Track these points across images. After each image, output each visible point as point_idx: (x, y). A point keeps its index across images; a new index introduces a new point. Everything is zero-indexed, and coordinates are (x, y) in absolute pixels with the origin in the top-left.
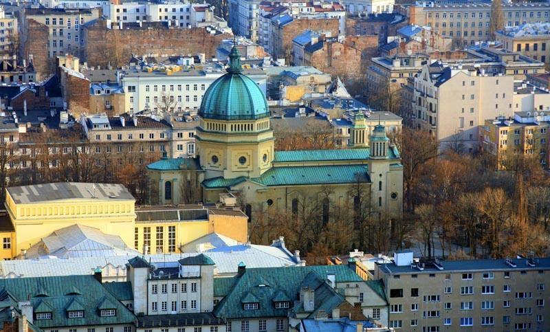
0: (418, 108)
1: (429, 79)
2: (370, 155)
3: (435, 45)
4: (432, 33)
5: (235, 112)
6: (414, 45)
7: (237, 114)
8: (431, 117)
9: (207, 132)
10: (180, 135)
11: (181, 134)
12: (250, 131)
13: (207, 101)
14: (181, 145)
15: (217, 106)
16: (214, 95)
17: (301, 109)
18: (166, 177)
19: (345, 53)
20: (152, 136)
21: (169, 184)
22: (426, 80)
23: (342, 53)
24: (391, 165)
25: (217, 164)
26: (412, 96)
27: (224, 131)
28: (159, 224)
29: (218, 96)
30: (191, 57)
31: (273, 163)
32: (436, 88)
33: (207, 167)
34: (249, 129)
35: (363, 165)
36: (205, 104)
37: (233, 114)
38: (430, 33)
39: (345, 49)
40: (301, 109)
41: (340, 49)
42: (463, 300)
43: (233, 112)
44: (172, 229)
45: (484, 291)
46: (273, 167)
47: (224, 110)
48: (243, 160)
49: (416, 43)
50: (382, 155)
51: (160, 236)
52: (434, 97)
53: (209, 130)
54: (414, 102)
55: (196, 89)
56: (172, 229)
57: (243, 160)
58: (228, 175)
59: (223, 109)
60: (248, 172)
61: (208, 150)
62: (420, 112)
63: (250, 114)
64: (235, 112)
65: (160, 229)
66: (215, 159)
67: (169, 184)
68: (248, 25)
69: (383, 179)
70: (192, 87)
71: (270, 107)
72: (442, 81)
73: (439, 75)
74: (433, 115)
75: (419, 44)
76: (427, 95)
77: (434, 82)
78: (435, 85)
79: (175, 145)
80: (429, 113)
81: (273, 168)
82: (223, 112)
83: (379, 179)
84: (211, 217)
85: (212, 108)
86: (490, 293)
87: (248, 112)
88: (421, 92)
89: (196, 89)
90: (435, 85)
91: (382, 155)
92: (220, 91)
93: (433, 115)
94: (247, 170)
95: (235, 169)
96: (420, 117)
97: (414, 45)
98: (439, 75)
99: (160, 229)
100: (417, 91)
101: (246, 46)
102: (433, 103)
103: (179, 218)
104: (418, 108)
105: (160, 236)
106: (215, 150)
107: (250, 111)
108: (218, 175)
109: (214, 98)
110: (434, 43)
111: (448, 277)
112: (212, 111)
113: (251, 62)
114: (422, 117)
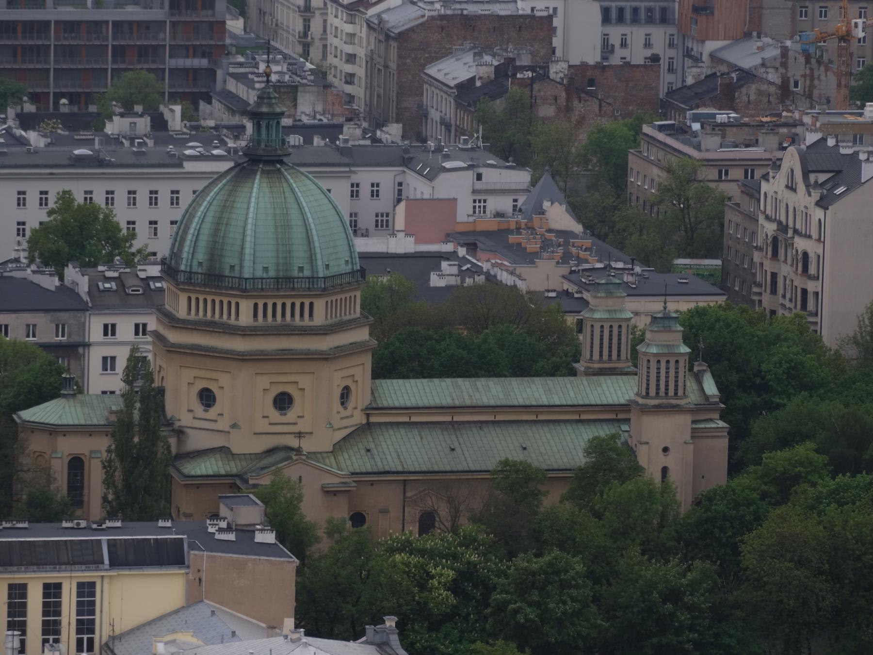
0: (769, 266)
1: (801, 187)
2: (637, 394)
3: (816, 93)
4: (808, 61)
5: (266, 269)
6: (760, 93)
7: (272, 274)
8: (805, 292)
9: (184, 321)
10: (109, 330)
11: (114, 326)
12: (307, 322)
13: (189, 237)
14: (113, 359)
15: (215, 252)
16: (211, 214)
17: (444, 264)
18: (68, 446)
19: (568, 109)
20: (31, 330)
21: (76, 465)
22: (791, 188)
23: (559, 109)
24: (694, 422)
25: (213, 413)
26: (754, 234)
27: (233, 321)
28: (52, 577)
29: (218, 224)
30: (141, 116)
31: (369, 411)
32: (819, 213)
33: (185, 420)
34: (302, 315)
35: (618, 421)
36: (181, 245)
37: (259, 273)
38: (802, 60)
39: (568, 100)
40: (444, 264)
41: (556, 99)
42: (475, 198)
43: (259, 267)
44: (86, 590)
45: (28, 336)
46: (368, 423)
47: (235, 261)
48: (283, 402)
49: (764, 87)
50: (671, 392)
51: (52, 608)
52: (815, 235)
53: (193, 316)
54: (759, 249)
55: (153, 201)
56: (86, 590)
57: (283, 402)
58: (245, 444)
59: (231, 260)
60: (300, 435)
61: (187, 375)
62: (774, 276)
63: (307, 273)
64: (266, 269)
65: (52, 591)
66: (207, 398)
67: (76, 465)
68: (300, 27)
69: (669, 461)
70: (143, 198)
71: (364, 256)
72: (838, 191)
73: (830, 175)
74: (811, 286)
75: (772, 89)
76: (796, 231)
77: (816, 195)
78: (818, 204)
79: (95, 357)
80: (799, 282)
81: (368, 427)
82: (232, 267)
83: (662, 460)
84: (192, 556)
85: (201, 256)
86: (31, 339)
87: (301, 269)
88: (780, 223)
89: (153, 201)
90: (818, 204)
91: (671, 392)
92: (226, 208)
93: (811, 286)
94: (296, 429)
95: (262, 425)
96: (774, 291)
97: (760, 93)
98: (830, 175)
99: (52, 591)
100: (768, 218)
101: (296, 87)
102: (812, 255)
103: (107, 561)
104: (769, 266)
105: (52, 608)
106: (208, 374)
107: (307, 267)
108: (217, 441)
109: (207, 229)
110: (812, 86)
111: (533, 9)
112: (200, 264)
113: (307, 131)
114: (780, 291)
